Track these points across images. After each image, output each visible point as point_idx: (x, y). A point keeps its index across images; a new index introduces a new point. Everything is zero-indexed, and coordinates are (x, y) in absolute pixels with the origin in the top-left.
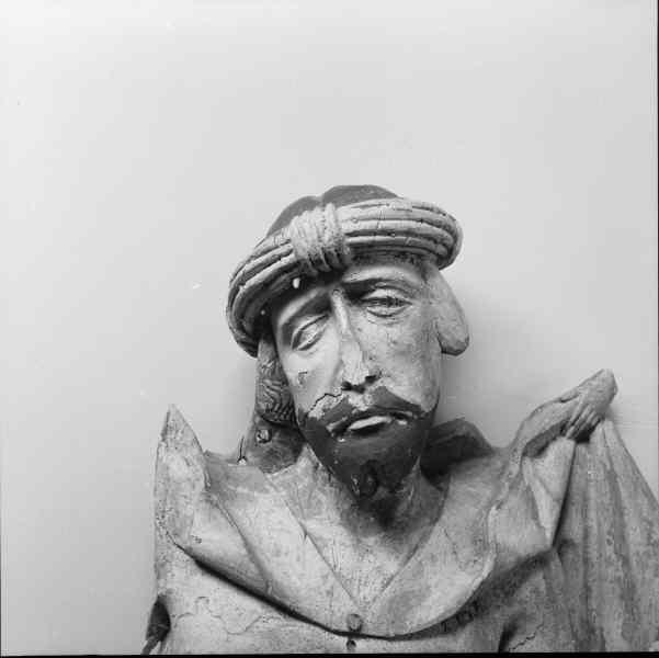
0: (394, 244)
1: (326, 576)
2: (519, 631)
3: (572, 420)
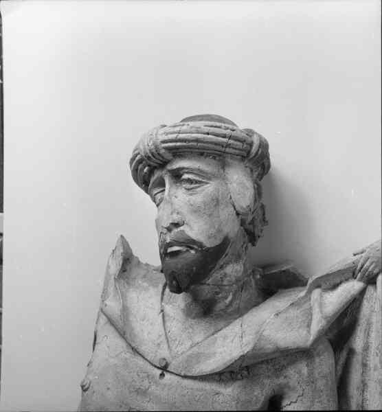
0: (189, 147)
1: (160, 336)
2: (286, 396)
3: (358, 268)
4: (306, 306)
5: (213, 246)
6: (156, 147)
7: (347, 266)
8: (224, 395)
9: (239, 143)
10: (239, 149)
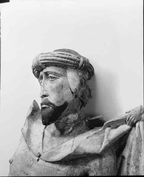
3: (127, 119)
4: (102, 135)
5: (59, 106)
6: (38, 62)
7: (122, 118)
8: (61, 171)
9: (72, 61)
10: (73, 64)
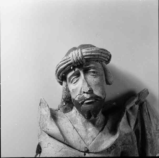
1: (79, 138)
